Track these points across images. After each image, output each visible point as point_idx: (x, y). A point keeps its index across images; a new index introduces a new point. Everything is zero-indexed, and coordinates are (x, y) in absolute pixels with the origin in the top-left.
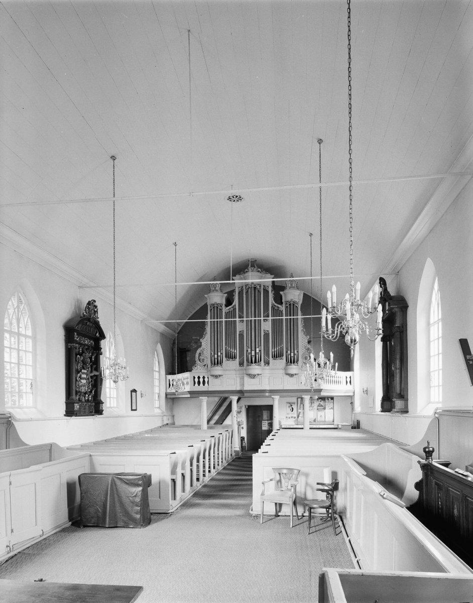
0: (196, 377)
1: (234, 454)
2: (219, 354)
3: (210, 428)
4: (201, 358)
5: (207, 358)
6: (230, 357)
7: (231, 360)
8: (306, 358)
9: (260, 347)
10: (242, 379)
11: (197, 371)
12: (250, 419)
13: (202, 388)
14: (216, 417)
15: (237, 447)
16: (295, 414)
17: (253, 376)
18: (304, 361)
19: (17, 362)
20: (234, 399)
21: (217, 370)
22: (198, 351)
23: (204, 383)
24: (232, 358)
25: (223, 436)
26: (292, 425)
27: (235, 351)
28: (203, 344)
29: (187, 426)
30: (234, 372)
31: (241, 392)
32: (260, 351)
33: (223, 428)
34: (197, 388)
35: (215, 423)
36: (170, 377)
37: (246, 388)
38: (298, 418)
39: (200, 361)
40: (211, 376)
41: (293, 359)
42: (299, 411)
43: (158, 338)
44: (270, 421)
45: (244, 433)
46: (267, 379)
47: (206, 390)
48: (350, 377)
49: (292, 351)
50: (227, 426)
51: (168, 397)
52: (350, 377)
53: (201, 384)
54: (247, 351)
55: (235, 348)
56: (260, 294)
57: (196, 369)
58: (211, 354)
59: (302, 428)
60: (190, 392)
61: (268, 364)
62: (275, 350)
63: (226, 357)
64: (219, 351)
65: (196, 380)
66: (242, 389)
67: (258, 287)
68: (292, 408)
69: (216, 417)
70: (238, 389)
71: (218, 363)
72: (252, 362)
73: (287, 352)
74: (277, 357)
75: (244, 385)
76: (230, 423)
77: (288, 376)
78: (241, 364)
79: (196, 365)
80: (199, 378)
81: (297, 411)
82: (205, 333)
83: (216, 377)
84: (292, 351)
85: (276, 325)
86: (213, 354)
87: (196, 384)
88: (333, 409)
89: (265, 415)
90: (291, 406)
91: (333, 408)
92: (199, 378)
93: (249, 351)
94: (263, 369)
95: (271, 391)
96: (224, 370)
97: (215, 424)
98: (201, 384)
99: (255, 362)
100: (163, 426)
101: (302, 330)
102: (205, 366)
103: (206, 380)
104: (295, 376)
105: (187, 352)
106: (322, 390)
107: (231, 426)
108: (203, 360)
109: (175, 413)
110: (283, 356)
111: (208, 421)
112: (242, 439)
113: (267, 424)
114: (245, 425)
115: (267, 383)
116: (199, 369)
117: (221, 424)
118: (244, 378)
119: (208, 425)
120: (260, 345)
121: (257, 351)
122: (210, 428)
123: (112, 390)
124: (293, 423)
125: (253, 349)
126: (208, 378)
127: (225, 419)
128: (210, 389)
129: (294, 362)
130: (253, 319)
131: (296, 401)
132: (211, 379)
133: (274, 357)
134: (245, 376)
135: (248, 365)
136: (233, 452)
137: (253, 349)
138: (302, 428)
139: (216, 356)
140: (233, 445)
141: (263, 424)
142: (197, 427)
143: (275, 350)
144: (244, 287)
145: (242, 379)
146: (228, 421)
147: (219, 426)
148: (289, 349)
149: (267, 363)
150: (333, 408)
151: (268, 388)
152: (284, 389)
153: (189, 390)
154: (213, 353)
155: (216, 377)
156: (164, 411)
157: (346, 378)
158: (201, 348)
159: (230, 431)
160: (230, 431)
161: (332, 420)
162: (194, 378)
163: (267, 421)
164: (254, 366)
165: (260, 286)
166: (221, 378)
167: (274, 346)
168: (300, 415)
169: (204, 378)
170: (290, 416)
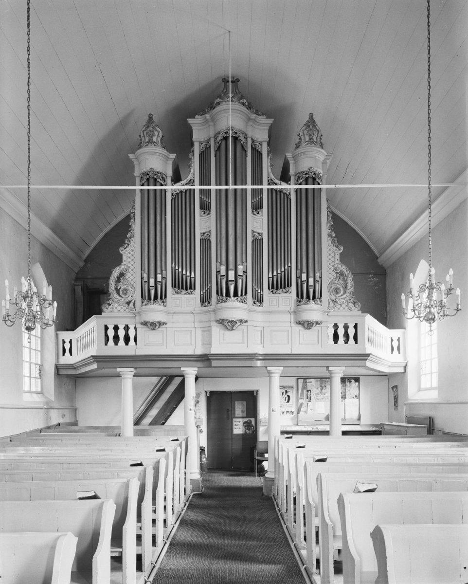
0: (111, 327)
1: (189, 488)
2: (159, 277)
3: (138, 433)
4: (122, 286)
5: (133, 287)
6: (182, 285)
7: (184, 292)
8: (337, 291)
9: (245, 264)
10: (207, 330)
11: (112, 314)
12: (213, 416)
13: (121, 349)
14: (154, 412)
15: (195, 473)
16: (292, 406)
17: (229, 325)
18: (334, 298)
19: (29, 375)
20: (190, 372)
21: (155, 312)
22: (116, 273)
23: (127, 340)
24: (186, 289)
25: (167, 458)
26: (287, 426)
27: (193, 276)
28: (124, 258)
29: (96, 428)
30: (190, 318)
31: (205, 359)
32: (245, 272)
33: (167, 433)
34: (112, 350)
35: (153, 423)
36: (66, 335)
37: (216, 349)
38: (298, 413)
39: (118, 293)
40: (144, 324)
41: (311, 291)
42: (300, 401)
43: (37, 251)
44: (246, 420)
45: (204, 443)
46: (259, 334)
47: (132, 353)
48: (398, 340)
49: (311, 274)
50: (175, 429)
51: (62, 372)
52: (398, 340)
53: (122, 342)
54: (218, 272)
55: (192, 268)
56: (246, 156)
57: (110, 309)
58: (142, 278)
59: (327, 433)
60: (97, 359)
61: (261, 301)
62: (275, 274)
63: (174, 285)
64: (159, 271)
65: (111, 333)
66: (207, 352)
67: (242, 138)
68: (289, 397)
69: (154, 412)
70: (199, 351)
71: (156, 298)
72: (228, 294)
73: (299, 277)
74: (277, 289)
75: (210, 344)
76: (182, 423)
77: (300, 328)
78: (205, 300)
79: (111, 302)
80: (116, 328)
81: (297, 401)
82: (128, 236)
83: (153, 326)
84: (311, 274)
85: (278, 222)
86: (146, 279)
87: (111, 342)
88: (359, 398)
89: (239, 408)
90: (286, 392)
91: (358, 397)
92: (116, 328)
93: (223, 272)
94: (250, 311)
95: (270, 358)
96: (169, 313)
97: (151, 424)
98: (122, 342)
99: (236, 294)
100: (48, 428)
101: (330, 235)
102: (128, 303)
103: (132, 333)
104: (314, 328)
105: (102, 296)
106: (368, 355)
107: (184, 428)
108: (126, 291)
109: (79, 404)
110: (290, 285)
111: (137, 422)
112: (202, 450)
113: (241, 424)
114: (204, 427)
115: (259, 342)
116: (116, 311)
117: (163, 424)
118: (210, 331)
119: (137, 427)
120: (244, 260)
121: (240, 273)
122: (138, 433)
123: (33, 380)
124: (290, 423)
125: (231, 266)
126: (135, 329)
127: (169, 416)
128: (140, 352)
129: (314, 298)
130: (231, 187)
131: (294, 384)
132: (142, 330)
133: (273, 288)
134: (214, 324)
135: (218, 302)
136: (188, 482)
137: (231, 266)
138: (327, 433)
139: (152, 282)
140: (188, 471)
141: (234, 423)
142: (114, 432)
143: (275, 274)
144: (212, 142)
145: (207, 330)
146: (176, 419)
147: (158, 429)
148: (304, 270)
149: (259, 299)
150: (358, 397)
151: (260, 350)
152: (293, 352)
153: (95, 354)
154: (145, 275)
155: (153, 326)
156: (52, 398)
157: (392, 340)
158: (122, 267)
159: (182, 439)
160: (182, 439)
161: (356, 416)
162: (106, 328)
163: (241, 420)
164: (232, 302)
165: (246, 138)
166: (162, 328)
167: (272, 267)
168: (302, 409)
169: (127, 328)
170: (285, 410)
